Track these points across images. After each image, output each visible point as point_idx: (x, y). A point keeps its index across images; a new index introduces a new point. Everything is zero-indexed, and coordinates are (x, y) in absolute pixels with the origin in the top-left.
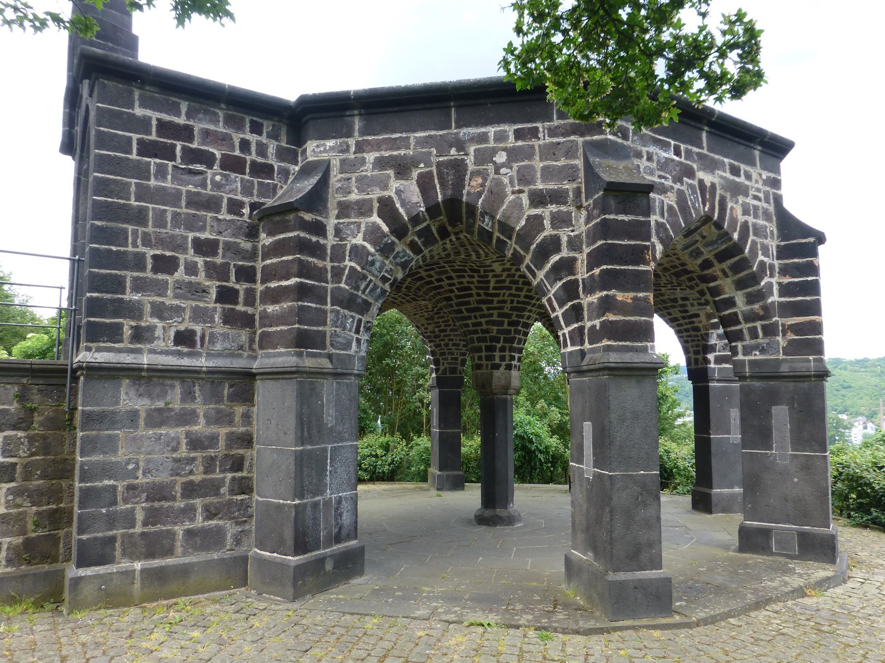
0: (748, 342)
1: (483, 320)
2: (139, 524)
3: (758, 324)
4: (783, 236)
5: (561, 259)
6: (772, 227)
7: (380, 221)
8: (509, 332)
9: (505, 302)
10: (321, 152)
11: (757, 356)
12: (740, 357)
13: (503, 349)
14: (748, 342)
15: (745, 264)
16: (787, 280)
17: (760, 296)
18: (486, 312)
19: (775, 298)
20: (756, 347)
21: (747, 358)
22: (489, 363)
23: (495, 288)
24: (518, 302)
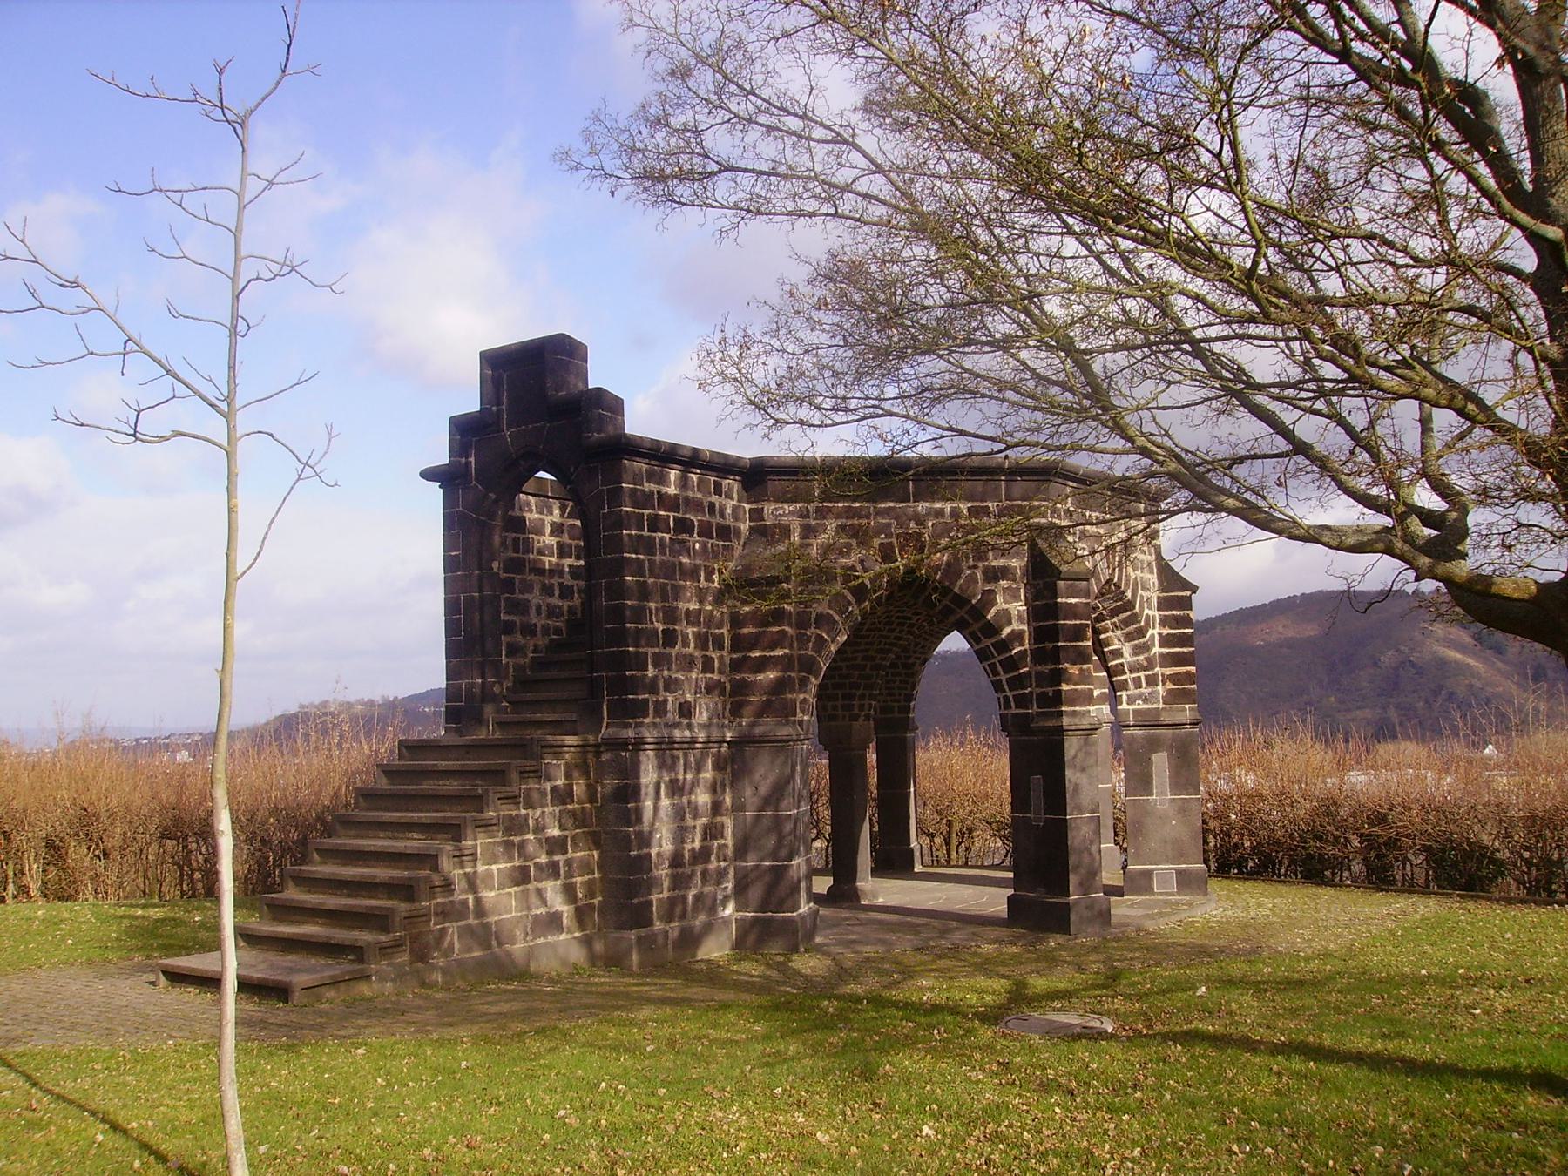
3: (1142, 674)
4: (1163, 589)
6: (1153, 578)
9: (872, 644)
12: (1124, 706)
13: (862, 697)
15: (1134, 619)
16: (1166, 631)
17: (1146, 648)
19: (1156, 650)
20: (1139, 696)
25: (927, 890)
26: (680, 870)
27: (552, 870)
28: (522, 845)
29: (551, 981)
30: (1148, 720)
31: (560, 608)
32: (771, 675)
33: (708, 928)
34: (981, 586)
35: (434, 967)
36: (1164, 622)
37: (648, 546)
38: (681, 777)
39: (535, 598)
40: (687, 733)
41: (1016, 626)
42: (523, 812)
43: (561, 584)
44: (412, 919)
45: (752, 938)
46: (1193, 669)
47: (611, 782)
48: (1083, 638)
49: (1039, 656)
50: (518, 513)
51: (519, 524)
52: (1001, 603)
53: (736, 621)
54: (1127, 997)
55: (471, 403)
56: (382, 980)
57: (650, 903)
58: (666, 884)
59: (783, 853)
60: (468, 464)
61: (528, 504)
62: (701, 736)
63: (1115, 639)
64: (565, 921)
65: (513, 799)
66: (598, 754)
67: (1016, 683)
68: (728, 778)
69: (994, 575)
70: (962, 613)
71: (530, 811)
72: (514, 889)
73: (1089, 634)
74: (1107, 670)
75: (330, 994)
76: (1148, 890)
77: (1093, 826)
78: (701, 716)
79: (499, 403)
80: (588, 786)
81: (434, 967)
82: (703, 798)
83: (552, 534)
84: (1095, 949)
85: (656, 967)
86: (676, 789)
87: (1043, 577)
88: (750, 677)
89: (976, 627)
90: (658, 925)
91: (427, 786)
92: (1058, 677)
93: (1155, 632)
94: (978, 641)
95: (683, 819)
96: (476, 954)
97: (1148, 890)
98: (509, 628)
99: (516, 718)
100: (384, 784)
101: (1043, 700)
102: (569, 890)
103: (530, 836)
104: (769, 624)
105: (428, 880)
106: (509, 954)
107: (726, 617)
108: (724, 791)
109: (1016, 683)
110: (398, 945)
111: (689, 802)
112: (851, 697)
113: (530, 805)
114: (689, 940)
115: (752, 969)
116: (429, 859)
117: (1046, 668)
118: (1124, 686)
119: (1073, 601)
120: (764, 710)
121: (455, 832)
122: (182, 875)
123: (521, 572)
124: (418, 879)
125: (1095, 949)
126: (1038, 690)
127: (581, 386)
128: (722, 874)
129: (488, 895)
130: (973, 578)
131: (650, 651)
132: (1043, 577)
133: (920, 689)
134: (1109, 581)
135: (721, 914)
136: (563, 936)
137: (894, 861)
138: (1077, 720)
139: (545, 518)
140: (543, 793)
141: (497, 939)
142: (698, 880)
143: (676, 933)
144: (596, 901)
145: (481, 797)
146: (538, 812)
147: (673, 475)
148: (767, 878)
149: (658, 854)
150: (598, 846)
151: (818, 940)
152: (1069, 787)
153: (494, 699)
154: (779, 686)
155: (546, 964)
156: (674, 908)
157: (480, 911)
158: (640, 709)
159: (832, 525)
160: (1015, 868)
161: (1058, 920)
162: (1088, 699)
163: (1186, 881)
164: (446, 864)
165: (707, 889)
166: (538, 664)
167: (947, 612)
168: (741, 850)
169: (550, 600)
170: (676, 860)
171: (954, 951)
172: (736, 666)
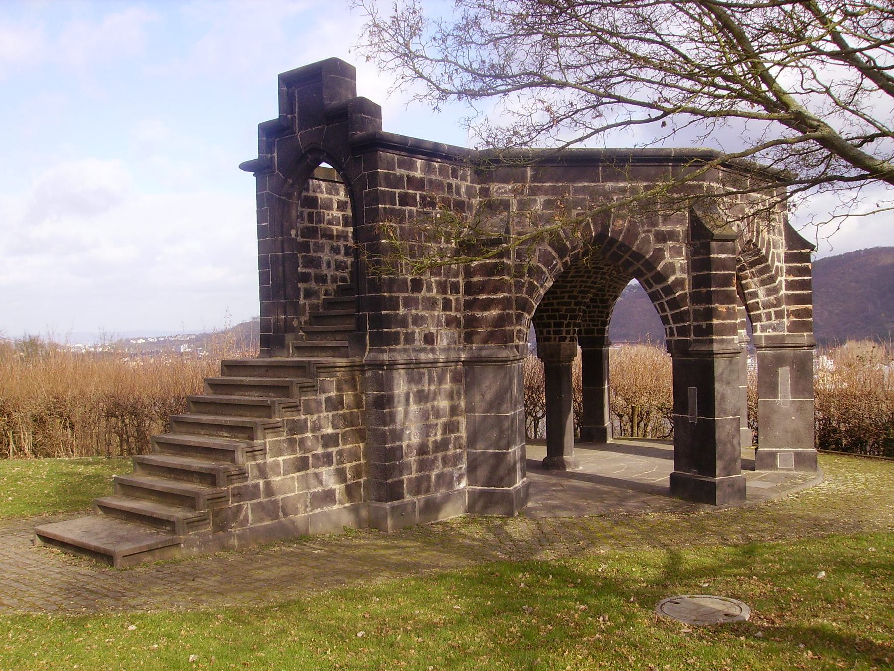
0: (765, 322)
1: (555, 301)
2: (414, 472)
3: (772, 310)
4: (789, 247)
5: (677, 279)
6: (781, 239)
7: (550, 249)
8: (574, 310)
9: (575, 287)
10: (502, 193)
11: (770, 333)
12: (759, 333)
13: (568, 325)
14: (765, 322)
15: (768, 269)
16: (791, 278)
17: (776, 290)
18: (559, 295)
19: (783, 292)
20: (770, 326)
21: (763, 334)
22: (557, 336)
23: (572, 277)
24: (585, 287)
25: (614, 460)
26: (425, 457)
27: (327, 459)
28: (302, 442)
29: (324, 543)
30: (777, 343)
31: (345, 263)
32: (495, 312)
33: (447, 498)
34: (654, 245)
35: (231, 535)
36: (789, 272)
37: (400, 217)
38: (426, 388)
39: (325, 256)
40: (431, 356)
41: (679, 275)
42: (303, 417)
43: (345, 246)
44: (216, 499)
45: (480, 504)
46: (810, 306)
47: (373, 393)
48: (729, 284)
49: (696, 298)
50: (311, 194)
51: (312, 202)
52: (668, 258)
53: (469, 273)
54: (761, 577)
55: (272, 113)
56: (189, 546)
57: (402, 482)
58: (414, 467)
59: (503, 442)
60: (272, 158)
61: (320, 187)
62: (442, 357)
63: (753, 284)
64: (337, 496)
65: (295, 408)
66: (363, 372)
67: (678, 318)
68: (462, 388)
69: (662, 237)
70: (638, 265)
71: (309, 416)
72: (298, 477)
73: (734, 281)
74: (747, 306)
75: (148, 558)
76: (773, 466)
77: (734, 425)
78: (442, 343)
79: (292, 112)
80: (356, 396)
81: (231, 535)
82: (443, 403)
83: (339, 208)
84: (734, 519)
85: (406, 531)
86: (422, 397)
87: (700, 237)
88: (479, 314)
89: (649, 276)
90: (408, 498)
91: (236, 397)
92: (710, 314)
93: (782, 279)
94: (650, 286)
95: (427, 419)
96: (266, 523)
97: (773, 466)
98: (305, 278)
99: (309, 343)
100: (208, 395)
101: (699, 331)
102: (340, 474)
103: (309, 435)
104: (493, 275)
105: (226, 470)
106: (293, 522)
107: (461, 270)
108: (459, 398)
109: (678, 318)
110: (202, 520)
111: (433, 407)
112: (560, 325)
113: (308, 411)
114: (432, 508)
115: (476, 531)
116: (228, 454)
117: (701, 307)
118: (759, 318)
119: (723, 256)
120: (490, 337)
121: (248, 432)
122: (121, 441)
123: (316, 237)
124: (218, 470)
125: (734, 519)
126: (695, 323)
127: (350, 97)
128: (457, 459)
129: (276, 479)
130: (646, 240)
131: (401, 295)
132: (700, 237)
133: (612, 316)
134: (751, 240)
135: (457, 487)
136: (336, 507)
137: (593, 435)
138: (724, 347)
139: (332, 197)
140: (319, 403)
141: (283, 511)
142: (439, 463)
143: (422, 503)
144: (362, 480)
145: (269, 407)
146: (315, 416)
147: (419, 163)
148: (491, 461)
149: (408, 446)
150: (362, 439)
151: (530, 505)
152: (717, 396)
153: (292, 330)
154: (500, 321)
155: (321, 528)
156: (419, 486)
157: (269, 491)
158: (393, 339)
159: (541, 199)
160: (676, 442)
161: (706, 494)
162: (733, 329)
163: (801, 461)
164: (240, 458)
165: (446, 470)
166: (329, 304)
167: (628, 264)
168: (472, 442)
169: (337, 257)
170: (422, 450)
171: (627, 520)
172: (469, 305)
